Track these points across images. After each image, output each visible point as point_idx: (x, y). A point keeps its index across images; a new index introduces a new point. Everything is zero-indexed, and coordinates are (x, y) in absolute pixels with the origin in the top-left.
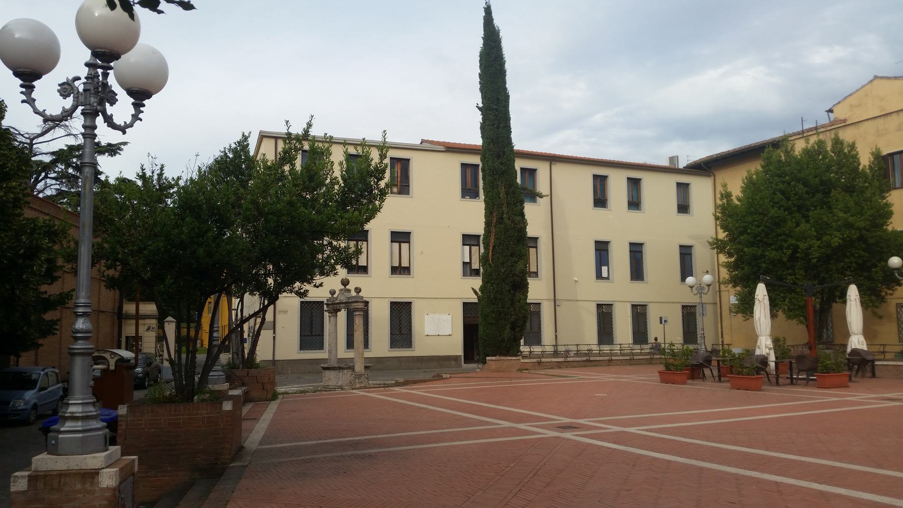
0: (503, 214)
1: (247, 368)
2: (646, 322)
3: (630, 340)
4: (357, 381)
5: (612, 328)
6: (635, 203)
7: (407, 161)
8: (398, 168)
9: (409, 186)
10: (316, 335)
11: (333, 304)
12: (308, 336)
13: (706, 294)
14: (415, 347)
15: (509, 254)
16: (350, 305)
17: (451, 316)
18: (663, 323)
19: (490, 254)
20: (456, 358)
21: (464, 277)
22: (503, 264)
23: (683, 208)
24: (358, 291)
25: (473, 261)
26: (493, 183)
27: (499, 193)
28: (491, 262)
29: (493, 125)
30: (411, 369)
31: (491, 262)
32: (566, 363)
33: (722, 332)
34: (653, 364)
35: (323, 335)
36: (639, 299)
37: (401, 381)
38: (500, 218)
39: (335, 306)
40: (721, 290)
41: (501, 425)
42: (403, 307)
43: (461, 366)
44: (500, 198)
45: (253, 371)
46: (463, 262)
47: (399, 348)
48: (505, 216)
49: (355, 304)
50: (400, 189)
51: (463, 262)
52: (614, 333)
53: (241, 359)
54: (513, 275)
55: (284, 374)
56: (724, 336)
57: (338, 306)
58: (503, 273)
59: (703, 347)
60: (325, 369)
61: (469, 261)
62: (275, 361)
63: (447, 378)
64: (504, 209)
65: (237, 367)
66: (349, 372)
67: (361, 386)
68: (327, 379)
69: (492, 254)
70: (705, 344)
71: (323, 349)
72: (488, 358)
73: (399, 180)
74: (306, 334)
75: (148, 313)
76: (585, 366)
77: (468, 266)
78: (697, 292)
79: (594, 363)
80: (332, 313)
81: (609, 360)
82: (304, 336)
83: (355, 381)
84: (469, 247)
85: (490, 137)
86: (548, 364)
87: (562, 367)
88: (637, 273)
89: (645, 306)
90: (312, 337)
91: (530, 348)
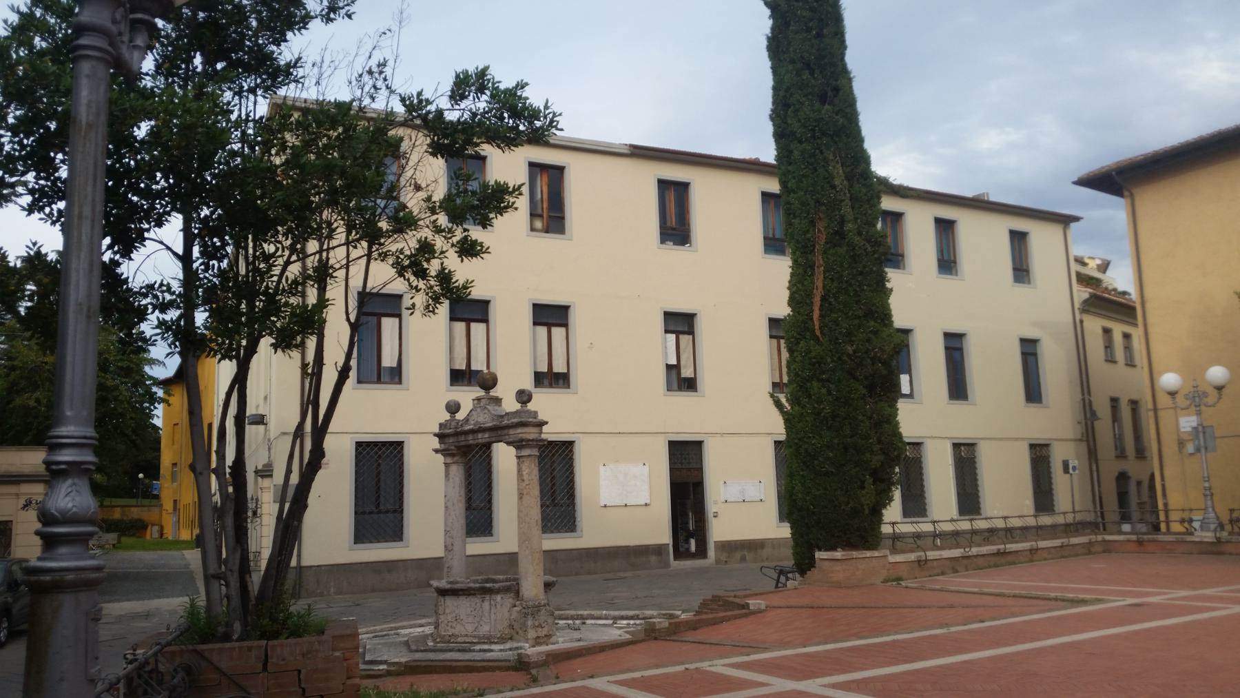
0: (842, 221)
1: (262, 637)
2: (975, 475)
3: (953, 511)
4: (530, 623)
5: (922, 486)
6: (947, 264)
7: (560, 170)
8: (542, 184)
9: (563, 218)
10: (387, 511)
11: (457, 434)
12: (370, 513)
13: (1213, 406)
14: (582, 531)
15: (860, 313)
16: (505, 432)
17: (647, 466)
18: (1071, 471)
19: (816, 314)
20: (659, 550)
21: (669, 392)
22: (849, 334)
23: (1021, 272)
24: (525, 399)
25: (682, 363)
26: (813, 155)
27: (829, 179)
28: (818, 333)
29: (809, 30)
30: (577, 574)
31: (818, 333)
32: (965, 561)
33: (1163, 486)
34: (1094, 554)
35: (402, 512)
36: (965, 433)
37: (662, 626)
38: (836, 233)
39: (463, 438)
40: (1159, 406)
41: (724, 665)
42: (557, 451)
43: (667, 565)
44: (834, 187)
45: (285, 650)
46: (667, 365)
47: (552, 532)
48: (849, 226)
49: (519, 430)
50: (547, 223)
51: (667, 365)
52: (926, 495)
53: (236, 602)
54: (874, 360)
55: (322, 595)
56: (1168, 492)
57: (470, 437)
58: (849, 356)
59: (1212, 515)
60: (443, 592)
61: (675, 363)
62: (301, 568)
63: (760, 612)
64: (847, 210)
65: (221, 630)
66: (508, 600)
67: (540, 634)
68: (449, 618)
69: (821, 316)
70: (1213, 509)
71: (401, 540)
72: (819, 555)
73: (545, 205)
74: (367, 510)
75: (27, 470)
76: (996, 566)
77: (674, 372)
78: (1188, 402)
79: (1009, 558)
80: (453, 455)
81: (1031, 550)
82: (364, 513)
83: (524, 625)
84: (674, 336)
85: (802, 57)
86: (935, 563)
87: (959, 569)
88: (958, 388)
89: (973, 445)
90: (372, 515)
91: (1232, 526)
